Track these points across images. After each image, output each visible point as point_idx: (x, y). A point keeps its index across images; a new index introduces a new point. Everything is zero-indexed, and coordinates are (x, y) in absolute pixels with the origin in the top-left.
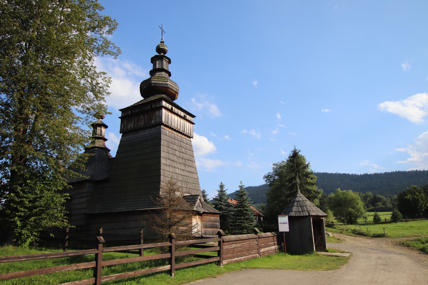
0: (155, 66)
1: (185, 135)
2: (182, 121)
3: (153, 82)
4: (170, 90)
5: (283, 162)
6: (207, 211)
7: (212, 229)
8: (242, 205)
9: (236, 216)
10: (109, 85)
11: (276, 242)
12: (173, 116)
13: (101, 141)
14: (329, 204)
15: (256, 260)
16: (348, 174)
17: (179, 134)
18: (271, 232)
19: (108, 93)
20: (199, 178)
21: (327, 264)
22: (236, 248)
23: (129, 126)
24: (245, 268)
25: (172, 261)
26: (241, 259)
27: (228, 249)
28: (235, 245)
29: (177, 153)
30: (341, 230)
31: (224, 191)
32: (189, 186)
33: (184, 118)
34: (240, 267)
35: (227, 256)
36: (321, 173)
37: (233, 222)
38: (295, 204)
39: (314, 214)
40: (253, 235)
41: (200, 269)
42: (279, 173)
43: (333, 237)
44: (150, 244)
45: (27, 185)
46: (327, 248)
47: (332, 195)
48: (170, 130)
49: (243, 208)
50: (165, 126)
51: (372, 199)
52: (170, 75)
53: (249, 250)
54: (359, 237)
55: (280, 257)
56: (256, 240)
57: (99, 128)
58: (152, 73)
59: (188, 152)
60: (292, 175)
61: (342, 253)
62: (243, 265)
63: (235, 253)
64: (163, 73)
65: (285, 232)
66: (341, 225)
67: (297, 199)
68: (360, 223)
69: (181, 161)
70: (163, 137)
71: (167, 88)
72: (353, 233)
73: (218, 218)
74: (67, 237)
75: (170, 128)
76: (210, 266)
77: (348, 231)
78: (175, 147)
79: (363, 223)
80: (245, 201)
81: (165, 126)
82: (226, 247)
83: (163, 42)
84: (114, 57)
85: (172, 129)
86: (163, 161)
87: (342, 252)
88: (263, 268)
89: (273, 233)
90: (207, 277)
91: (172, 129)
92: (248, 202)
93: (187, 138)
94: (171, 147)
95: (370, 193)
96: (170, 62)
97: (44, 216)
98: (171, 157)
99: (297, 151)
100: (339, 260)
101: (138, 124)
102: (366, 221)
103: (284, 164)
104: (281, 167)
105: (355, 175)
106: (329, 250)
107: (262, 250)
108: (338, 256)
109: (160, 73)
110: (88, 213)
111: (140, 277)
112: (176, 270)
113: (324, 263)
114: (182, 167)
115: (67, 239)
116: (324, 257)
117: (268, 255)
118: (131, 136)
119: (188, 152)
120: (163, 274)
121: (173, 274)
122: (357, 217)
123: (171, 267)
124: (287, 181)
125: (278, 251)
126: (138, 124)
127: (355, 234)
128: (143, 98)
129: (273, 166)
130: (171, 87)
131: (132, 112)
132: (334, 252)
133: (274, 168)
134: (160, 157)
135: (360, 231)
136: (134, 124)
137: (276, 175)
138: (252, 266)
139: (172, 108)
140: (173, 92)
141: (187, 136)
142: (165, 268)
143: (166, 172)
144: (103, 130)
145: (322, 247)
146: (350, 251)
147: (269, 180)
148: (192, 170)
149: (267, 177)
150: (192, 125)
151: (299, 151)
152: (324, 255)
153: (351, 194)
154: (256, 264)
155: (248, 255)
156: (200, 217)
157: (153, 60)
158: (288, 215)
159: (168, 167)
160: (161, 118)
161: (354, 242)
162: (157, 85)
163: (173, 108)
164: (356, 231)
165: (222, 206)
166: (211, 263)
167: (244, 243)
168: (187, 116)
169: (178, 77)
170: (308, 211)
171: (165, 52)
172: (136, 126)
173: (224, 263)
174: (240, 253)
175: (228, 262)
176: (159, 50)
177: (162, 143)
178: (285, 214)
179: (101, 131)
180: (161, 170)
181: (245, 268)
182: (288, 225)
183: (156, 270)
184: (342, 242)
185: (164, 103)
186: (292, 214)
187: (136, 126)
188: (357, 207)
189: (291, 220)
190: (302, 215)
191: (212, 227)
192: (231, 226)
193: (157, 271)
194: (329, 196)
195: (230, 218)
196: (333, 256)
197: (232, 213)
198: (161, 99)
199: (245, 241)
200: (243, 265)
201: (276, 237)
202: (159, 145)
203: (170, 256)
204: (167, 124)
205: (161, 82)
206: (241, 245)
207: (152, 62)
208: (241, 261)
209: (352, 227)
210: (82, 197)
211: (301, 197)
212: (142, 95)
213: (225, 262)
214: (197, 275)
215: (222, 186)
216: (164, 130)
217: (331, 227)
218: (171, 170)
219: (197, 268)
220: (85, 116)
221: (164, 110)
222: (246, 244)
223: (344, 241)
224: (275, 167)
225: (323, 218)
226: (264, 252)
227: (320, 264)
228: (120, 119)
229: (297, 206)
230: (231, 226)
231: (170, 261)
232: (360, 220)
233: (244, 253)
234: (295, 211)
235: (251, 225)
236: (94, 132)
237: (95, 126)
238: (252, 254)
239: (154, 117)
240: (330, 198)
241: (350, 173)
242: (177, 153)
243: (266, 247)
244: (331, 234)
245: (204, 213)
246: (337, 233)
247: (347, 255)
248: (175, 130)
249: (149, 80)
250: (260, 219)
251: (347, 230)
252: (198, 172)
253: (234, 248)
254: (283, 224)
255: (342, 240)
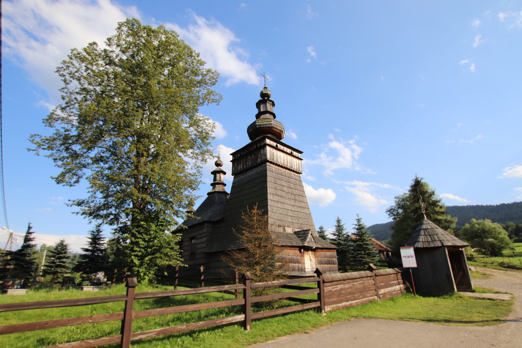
0: (259, 109)
1: (294, 171)
2: (289, 157)
3: (257, 124)
4: (274, 129)
5: (405, 194)
6: (320, 246)
7: (329, 265)
8: (361, 239)
9: (356, 251)
10: (214, 130)
11: (401, 281)
12: (279, 153)
13: (221, 186)
14: (464, 236)
15: (374, 304)
16: (482, 206)
17: (287, 171)
18: (393, 268)
19: (214, 138)
20: (312, 213)
21: (479, 313)
22: (344, 289)
23: (239, 167)
24: (356, 317)
25: (254, 310)
26: (352, 304)
27: (331, 291)
28: (342, 285)
29: (285, 189)
30: (484, 263)
31: (342, 226)
32: (301, 222)
33: (291, 154)
34: (349, 315)
35: (331, 300)
36: (450, 207)
37: (353, 257)
38: (422, 232)
39: (450, 244)
40: (368, 273)
41: (290, 319)
42: (402, 206)
43: (477, 272)
44: (212, 287)
45: (141, 226)
46: (473, 287)
47: (467, 226)
48: (277, 167)
49: (363, 242)
50: (271, 163)
51: (514, 229)
52: (275, 117)
53: (363, 291)
54: (511, 271)
55: (407, 300)
56: (372, 278)
57: (218, 175)
58: (258, 116)
59: (298, 187)
60: (417, 206)
61: (498, 295)
62: (354, 312)
63: (341, 296)
64: (268, 115)
65: (412, 268)
66: (483, 257)
67: (424, 227)
68: (506, 255)
69: (290, 196)
70: (269, 174)
71: (272, 127)
72: (500, 266)
73: (335, 253)
74: (177, 275)
75: (276, 165)
76: (307, 314)
77: (493, 265)
78: (283, 183)
79: (510, 254)
80: (363, 234)
81: (271, 163)
82: (327, 289)
83: (266, 88)
84: (216, 103)
85: (279, 166)
86: (270, 197)
87: (497, 293)
88: (382, 318)
89: (396, 269)
90: (297, 331)
91: (279, 166)
92: (367, 236)
93: (296, 174)
94: (278, 183)
95: (511, 223)
96: (273, 104)
97: (158, 255)
98: (279, 193)
99: (419, 179)
100: (497, 305)
101: (246, 165)
102: (514, 253)
103: (406, 196)
104: (403, 200)
105: (490, 206)
106: (476, 290)
107: (382, 291)
108: (492, 300)
109: (265, 115)
110: (207, 251)
111: (200, 331)
112: (252, 320)
113: (474, 310)
114: (292, 203)
115: (177, 277)
116: (472, 300)
117: (392, 297)
118: (242, 177)
119: (298, 187)
120: (236, 326)
121: (248, 327)
122: (501, 248)
123: (246, 317)
124: (411, 212)
125: (405, 291)
126: (246, 165)
127: (504, 267)
128: (250, 141)
129: (395, 199)
130: (275, 126)
131: (241, 154)
132: (484, 292)
133: (396, 201)
134: (267, 193)
135: (511, 264)
136: (243, 165)
137: (399, 208)
138: (367, 314)
139: (277, 146)
140: (277, 131)
141: (296, 172)
142: (237, 319)
143: (274, 208)
144: (222, 176)
145: (465, 285)
146: (509, 292)
147: (392, 213)
148: (303, 205)
149: (391, 211)
150: (300, 161)
151: (422, 179)
152: (471, 297)
153: (488, 223)
154: (373, 311)
155: (362, 298)
156: (313, 252)
157: (258, 105)
158: (414, 246)
159: (276, 203)
160: (266, 155)
161: (507, 278)
162: (262, 126)
163: (278, 145)
164: (504, 264)
165: (341, 242)
166: (308, 310)
167: (355, 283)
168: (294, 152)
169: (283, 118)
170: (441, 241)
171: (268, 96)
172: (245, 167)
173: (326, 310)
174: (352, 295)
175: (333, 309)
176: (263, 95)
177: (268, 180)
178: (409, 245)
179: (220, 178)
180: (269, 206)
181: (356, 317)
182: (414, 258)
183: (222, 322)
184: (491, 278)
185: (268, 141)
186: (419, 245)
187: (245, 167)
188: (500, 236)
189: (417, 251)
190: (432, 245)
191: (329, 263)
192: (352, 261)
193: (224, 323)
194: (463, 227)
195: (349, 254)
196: (484, 299)
197: (352, 248)
198: (264, 139)
199: (356, 280)
200: (354, 312)
201: (400, 274)
202: (266, 182)
203: (244, 303)
204: (273, 161)
205: (265, 123)
206: (351, 285)
207: (257, 108)
208: (352, 306)
209: (499, 259)
210: (203, 237)
211: (428, 224)
212: (250, 139)
213: (328, 308)
214: (283, 328)
215: (339, 221)
216: (269, 166)
217: (471, 261)
218: (280, 205)
219: (287, 317)
220: (194, 161)
221: (268, 148)
222: (357, 284)
223: (492, 277)
224: (397, 200)
225: (463, 249)
226: (385, 293)
227: (468, 312)
228: (231, 163)
229: (425, 235)
230: (352, 261)
231: (242, 309)
232: (505, 252)
233: (356, 295)
234: (422, 241)
235: (373, 260)
236: (215, 179)
237: (214, 173)
238: (367, 297)
239: (260, 156)
240: (466, 230)
241: (484, 204)
242: (285, 189)
243: (387, 287)
244: (473, 268)
245: (317, 248)
246: (480, 267)
247: (506, 297)
248: (282, 167)
249: (255, 122)
250: (388, 254)
251: (491, 263)
252: (310, 207)
253: (341, 289)
254: (408, 258)
255: (490, 275)
